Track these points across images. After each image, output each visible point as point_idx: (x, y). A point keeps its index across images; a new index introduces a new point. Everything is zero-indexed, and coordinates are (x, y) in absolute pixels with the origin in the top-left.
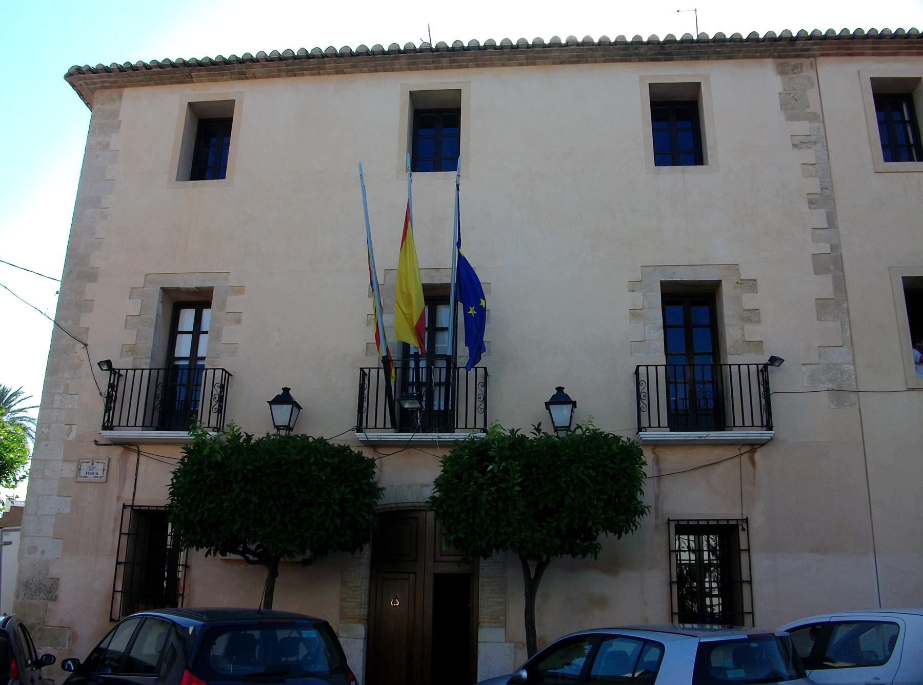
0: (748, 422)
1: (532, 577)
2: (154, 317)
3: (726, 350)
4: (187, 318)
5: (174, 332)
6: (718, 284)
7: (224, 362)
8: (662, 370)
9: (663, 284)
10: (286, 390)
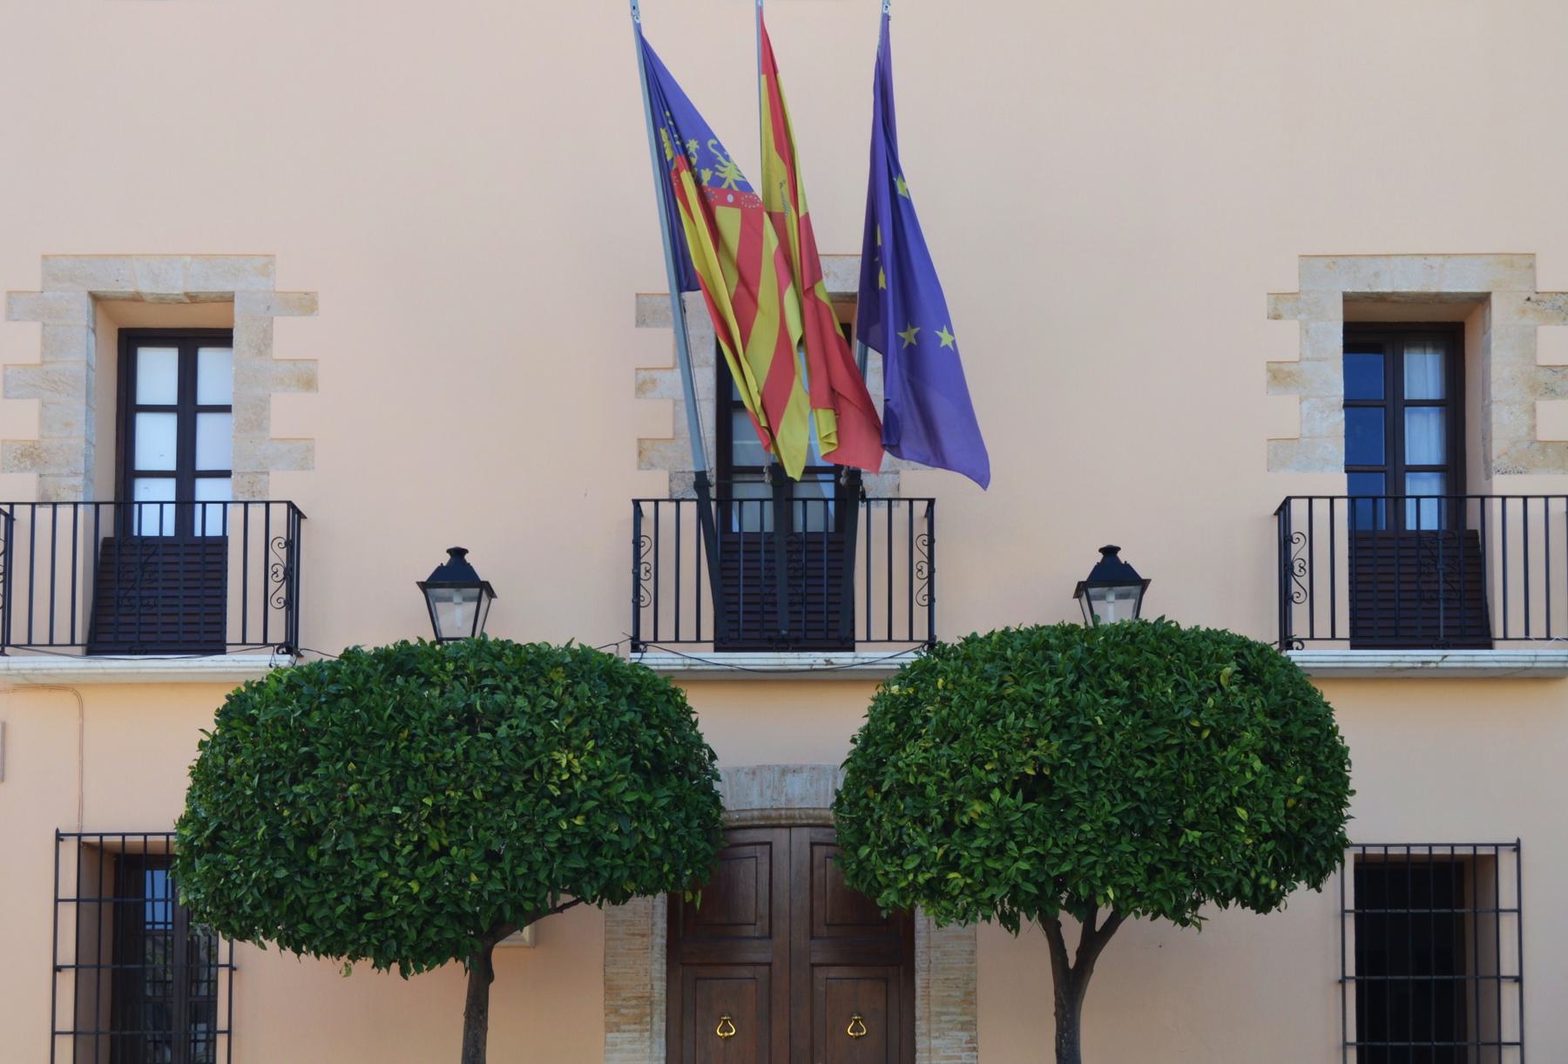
0: (41, 636)
1: (1071, 965)
2: (80, 369)
3: (1487, 461)
4: (157, 372)
5: (127, 409)
6: (1481, 301)
7: (282, 485)
8: (1342, 507)
9: (1349, 300)
10: (1110, 552)
